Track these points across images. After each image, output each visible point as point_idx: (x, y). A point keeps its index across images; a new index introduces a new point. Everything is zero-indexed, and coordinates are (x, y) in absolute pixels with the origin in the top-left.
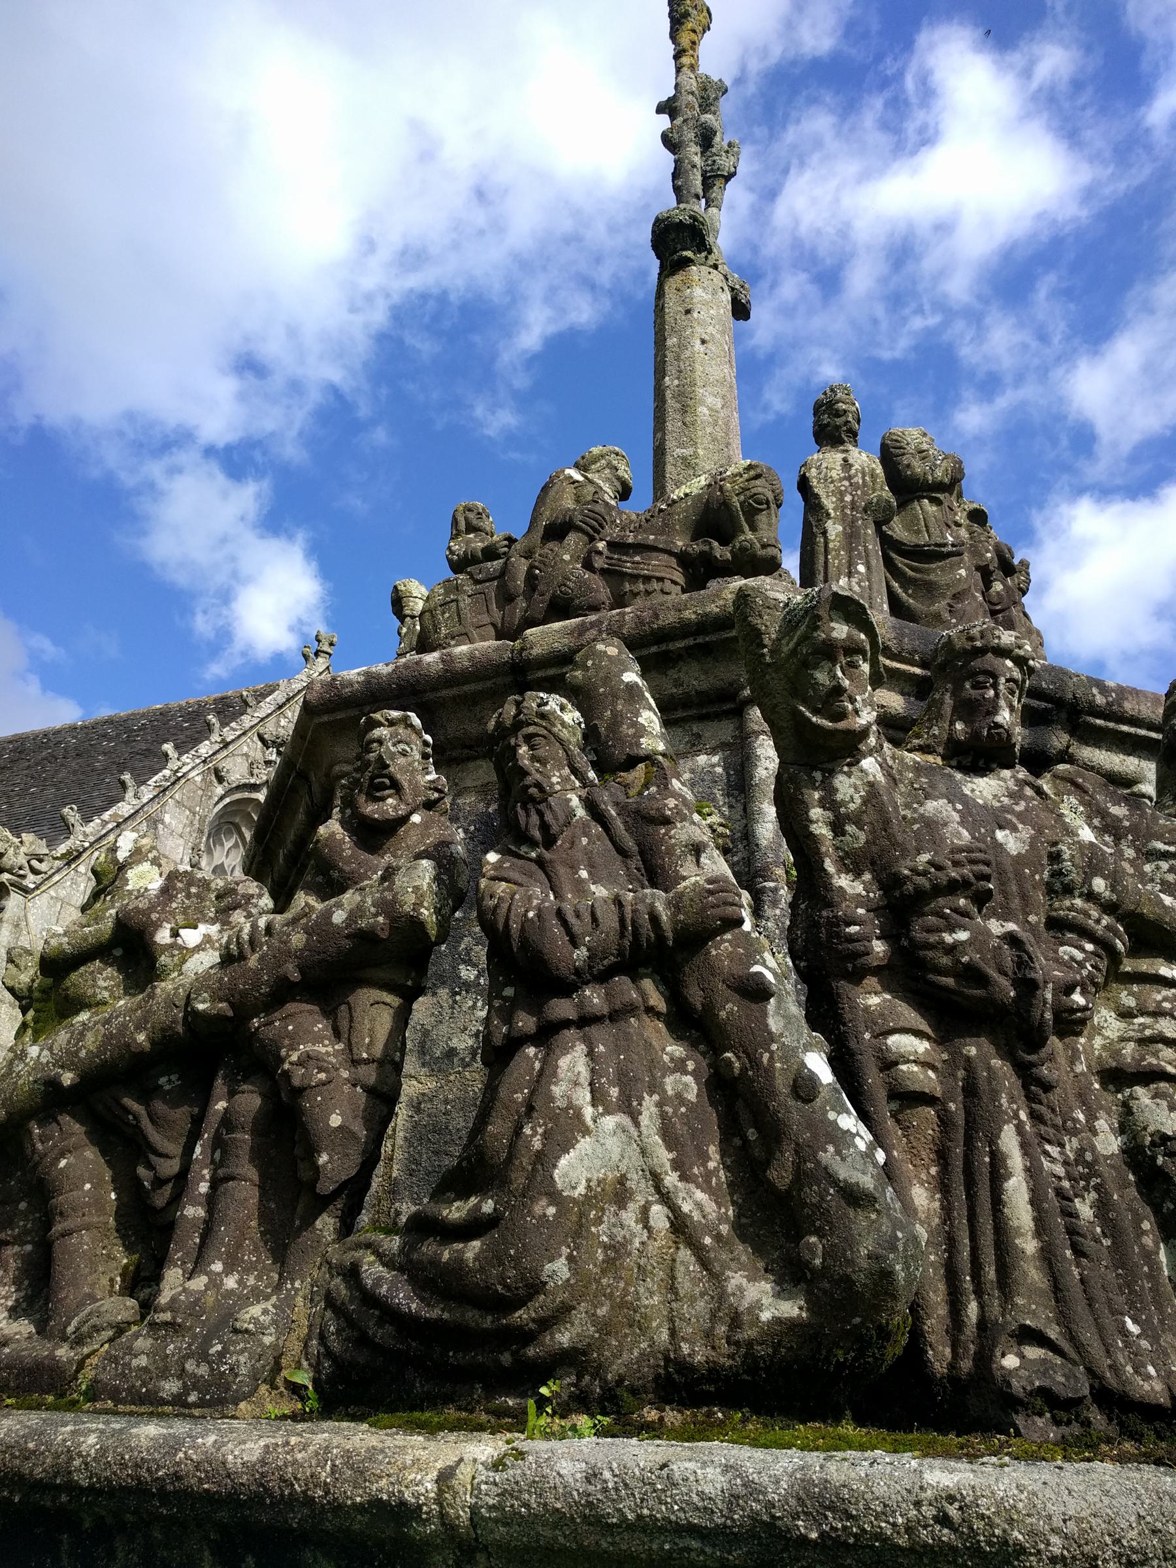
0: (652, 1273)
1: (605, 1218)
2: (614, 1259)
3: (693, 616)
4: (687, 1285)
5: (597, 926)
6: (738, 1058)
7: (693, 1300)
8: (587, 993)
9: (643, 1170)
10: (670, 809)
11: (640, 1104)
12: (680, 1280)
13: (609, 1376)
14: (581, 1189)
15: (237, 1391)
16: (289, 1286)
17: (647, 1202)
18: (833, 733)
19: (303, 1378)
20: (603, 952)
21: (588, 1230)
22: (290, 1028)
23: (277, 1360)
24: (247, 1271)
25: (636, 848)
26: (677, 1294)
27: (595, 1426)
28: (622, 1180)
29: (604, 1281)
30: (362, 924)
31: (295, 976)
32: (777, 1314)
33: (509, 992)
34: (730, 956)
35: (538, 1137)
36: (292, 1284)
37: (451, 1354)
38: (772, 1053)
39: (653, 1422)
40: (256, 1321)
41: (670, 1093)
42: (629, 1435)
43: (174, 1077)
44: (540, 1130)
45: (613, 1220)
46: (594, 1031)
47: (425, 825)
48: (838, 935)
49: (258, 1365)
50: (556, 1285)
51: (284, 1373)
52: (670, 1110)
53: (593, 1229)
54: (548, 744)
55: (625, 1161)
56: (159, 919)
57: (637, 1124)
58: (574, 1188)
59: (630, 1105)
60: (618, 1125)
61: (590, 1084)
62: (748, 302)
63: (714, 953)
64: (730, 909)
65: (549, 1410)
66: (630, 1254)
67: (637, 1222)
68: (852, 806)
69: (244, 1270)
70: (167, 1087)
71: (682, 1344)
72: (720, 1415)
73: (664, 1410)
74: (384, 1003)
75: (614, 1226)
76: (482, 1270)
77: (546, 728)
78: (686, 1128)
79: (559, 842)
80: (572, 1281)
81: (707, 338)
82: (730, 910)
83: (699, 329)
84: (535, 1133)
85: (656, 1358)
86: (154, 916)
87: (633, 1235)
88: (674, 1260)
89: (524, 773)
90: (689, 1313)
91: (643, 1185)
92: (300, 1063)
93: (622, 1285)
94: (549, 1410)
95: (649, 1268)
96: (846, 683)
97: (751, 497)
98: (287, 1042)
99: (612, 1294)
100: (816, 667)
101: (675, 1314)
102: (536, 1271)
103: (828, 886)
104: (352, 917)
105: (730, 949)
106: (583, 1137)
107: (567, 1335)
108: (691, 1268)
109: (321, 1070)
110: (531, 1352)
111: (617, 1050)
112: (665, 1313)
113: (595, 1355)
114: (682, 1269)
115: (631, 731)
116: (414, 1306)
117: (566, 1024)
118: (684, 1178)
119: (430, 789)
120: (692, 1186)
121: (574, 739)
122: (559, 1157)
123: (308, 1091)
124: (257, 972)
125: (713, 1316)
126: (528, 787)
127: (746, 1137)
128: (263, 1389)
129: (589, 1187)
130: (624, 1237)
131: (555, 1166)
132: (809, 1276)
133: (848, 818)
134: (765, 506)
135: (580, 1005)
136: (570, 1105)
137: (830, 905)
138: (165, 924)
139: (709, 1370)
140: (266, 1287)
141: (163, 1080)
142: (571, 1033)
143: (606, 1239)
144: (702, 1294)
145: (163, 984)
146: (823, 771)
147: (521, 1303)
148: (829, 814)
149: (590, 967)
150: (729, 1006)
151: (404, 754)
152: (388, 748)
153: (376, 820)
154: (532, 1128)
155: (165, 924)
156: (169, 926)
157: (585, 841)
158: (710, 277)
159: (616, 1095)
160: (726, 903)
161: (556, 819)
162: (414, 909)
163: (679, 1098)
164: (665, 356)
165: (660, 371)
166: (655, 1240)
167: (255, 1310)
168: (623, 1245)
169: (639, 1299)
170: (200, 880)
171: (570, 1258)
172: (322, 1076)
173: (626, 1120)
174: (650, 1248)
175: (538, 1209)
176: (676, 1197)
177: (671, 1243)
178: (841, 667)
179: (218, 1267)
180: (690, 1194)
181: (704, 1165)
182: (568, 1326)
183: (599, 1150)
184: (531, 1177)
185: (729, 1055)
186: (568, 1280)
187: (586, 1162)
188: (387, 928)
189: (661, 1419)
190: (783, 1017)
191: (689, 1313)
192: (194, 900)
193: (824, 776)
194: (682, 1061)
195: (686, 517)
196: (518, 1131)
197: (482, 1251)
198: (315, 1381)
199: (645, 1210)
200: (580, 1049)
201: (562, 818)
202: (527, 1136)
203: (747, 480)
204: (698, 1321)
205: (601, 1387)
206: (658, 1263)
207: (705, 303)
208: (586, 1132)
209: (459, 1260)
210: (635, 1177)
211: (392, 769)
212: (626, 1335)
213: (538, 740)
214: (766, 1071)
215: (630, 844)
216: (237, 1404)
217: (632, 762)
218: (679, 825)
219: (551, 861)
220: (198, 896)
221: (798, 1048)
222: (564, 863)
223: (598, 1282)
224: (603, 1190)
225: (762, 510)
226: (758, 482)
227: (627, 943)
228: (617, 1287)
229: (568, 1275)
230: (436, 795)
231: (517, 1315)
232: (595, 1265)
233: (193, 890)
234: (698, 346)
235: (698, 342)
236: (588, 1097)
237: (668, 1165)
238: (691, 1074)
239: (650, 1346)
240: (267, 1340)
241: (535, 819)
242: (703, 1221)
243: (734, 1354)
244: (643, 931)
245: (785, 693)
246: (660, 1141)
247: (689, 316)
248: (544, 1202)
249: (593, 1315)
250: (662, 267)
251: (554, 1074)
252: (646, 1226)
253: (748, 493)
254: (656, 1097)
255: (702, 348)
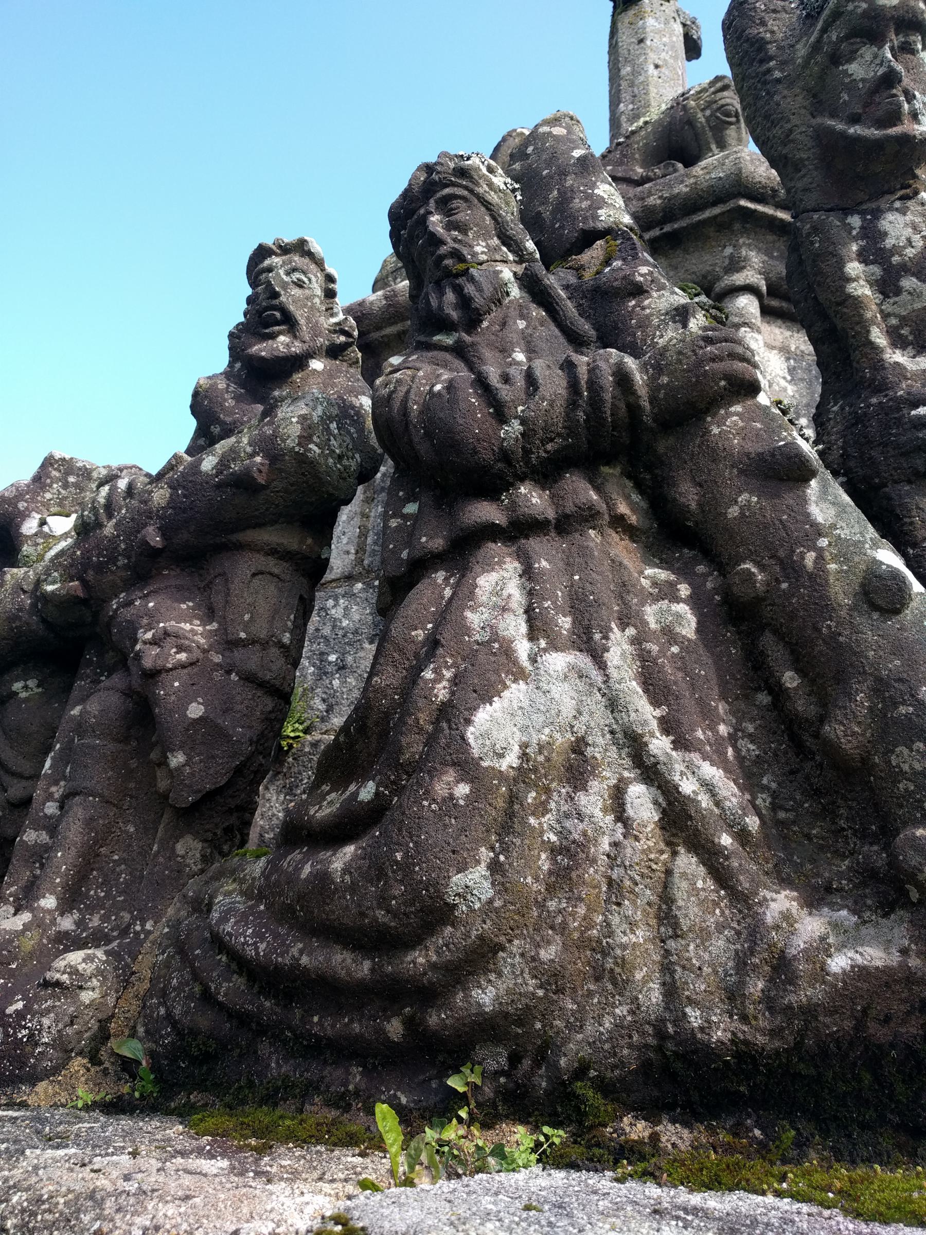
0: (632, 892)
1: (553, 805)
2: (568, 868)
3: (659, 202)
4: (694, 911)
5: (536, 389)
6: (762, 567)
7: (704, 936)
8: (523, 490)
9: (612, 732)
10: (642, 275)
11: (606, 637)
12: (680, 903)
13: (563, 1062)
14: (512, 759)
15: (34, 1067)
16: (138, 928)
17: (621, 780)
18: (878, 145)
19: (132, 1049)
20: (545, 429)
21: (524, 823)
22: (151, 604)
23: (104, 1024)
24: (91, 909)
25: (593, 333)
26: (676, 925)
27: (538, 1144)
28: (579, 746)
29: (552, 905)
30: (235, 467)
31: (156, 540)
32: (859, 960)
33: (411, 508)
34: (741, 432)
35: (445, 683)
36: (143, 925)
37: (316, 1019)
38: (820, 552)
39: (641, 1142)
40: (73, 971)
41: (653, 626)
42: (595, 1165)
43: (31, 683)
44: (448, 674)
45: (565, 808)
46: (534, 544)
47: (329, 374)
48: (899, 422)
49: (69, 1031)
50: (472, 910)
51: (112, 1043)
52: (654, 648)
53: (532, 821)
54: (469, 208)
55: (584, 718)
56: (27, 508)
57: (601, 665)
58: (501, 756)
59: (590, 639)
60: (572, 667)
61: (526, 612)
62: (699, 38)
63: (715, 430)
64: (740, 366)
65: (463, 1114)
66: (594, 861)
67: (605, 810)
68: (910, 252)
69: (87, 907)
70: (23, 695)
71: (688, 1010)
72: (757, 1132)
73: (659, 1122)
74: (271, 574)
75: (567, 816)
76: (353, 888)
77: (466, 188)
78: (680, 675)
79: (485, 324)
80: (498, 903)
81: (660, 63)
82: (740, 366)
83: (653, 57)
84: (439, 678)
85: (643, 1034)
86: (22, 505)
87: (599, 831)
88: (669, 872)
89: (436, 241)
90: (699, 958)
91: (613, 752)
92: (154, 642)
93: (582, 910)
94: (463, 1114)
95: (628, 883)
96: (899, 68)
97: (719, 109)
98: (145, 621)
99: (564, 926)
100: (851, 57)
101: (674, 958)
102: (437, 887)
103: (879, 365)
104: (223, 464)
105: (741, 424)
106: (515, 681)
107: (491, 992)
108: (700, 884)
109: (180, 649)
110: (434, 1019)
111: (569, 567)
112: (657, 958)
113: (538, 1026)
114: (684, 885)
115: (585, 204)
116: (262, 946)
117: (490, 532)
118: (680, 744)
119: (335, 332)
120: (695, 757)
121: (510, 210)
122: (476, 709)
123: (164, 675)
124: (113, 540)
125: (742, 964)
126: (442, 258)
127: (780, 685)
128: (78, 1064)
129: (524, 756)
130: (585, 834)
131: (468, 722)
132: (914, 895)
133: (906, 269)
134: (733, 119)
135: (513, 506)
136: (495, 637)
137: (881, 387)
138: (34, 514)
139: (739, 1056)
140: (112, 930)
141: (17, 686)
142: (495, 548)
143: (553, 838)
144: (720, 928)
145: (15, 570)
146: (862, 213)
147: (415, 940)
148: (876, 270)
149: (527, 452)
150: (743, 498)
151: (299, 285)
152: (278, 274)
153: (263, 358)
154: (435, 671)
155: (34, 514)
156: (38, 516)
157: (521, 324)
158: (663, 8)
159: (567, 626)
160: (733, 356)
161: (480, 290)
162: (299, 444)
163: (669, 634)
164: (620, 85)
165: (615, 100)
166: (637, 839)
167: (75, 957)
168: (582, 846)
169: (611, 934)
170: (80, 469)
171: (495, 867)
172: (183, 656)
173: (584, 661)
174: (629, 851)
175: (440, 789)
176: (670, 771)
177: (662, 846)
178: (892, 49)
179: (49, 902)
180: (692, 769)
181: (713, 728)
182: (493, 977)
183: (541, 699)
184: (431, 740)
185: (747, 566)
186: (490, 901)
187: (519, 720)
188: (265, 469)
189: (655, 1138)
190: (833, 504)
191: (699, 958)
192: (73, 490)
193: (864, 220)
194: (672, 585)
195: (646, 145)
196: (415, 673)
197: (355, 857)
198: (152, 1054)
199: (618, 794)
200: (512, 567)
201: (488, 289)
202: (426, 682)
203: (715, 93)
204: (716, 972)
205: (549, 1079)
206: (642, 876)
207: (658, 32)
208: (520, 675)
209: (323, 878)
210: (600, 741)
211: (283, 299)
212: (590, 994)
213: (455, 203)
214: (811, 576)
215: (586, 327)
216: (34, 1085)
217: (589, 237)
218: (655, 294)
219: (473, 344)
220: (76, 485)
221: (864, 542)
222: (491, 345)
223: (541, 906)
224: (548, 760)
225: (731, 123)
226: (725, 93)
227: (581, 415)
228: (573, 915)
229: (490, 893)
230: (342, 339)
231: (409, 958)
232: (536, 879)
233: (72, 479)
234: (651, 69)
235: (652, 67)
236: (523, 628)
237: (654, 725)
238: (684, 601)
239: (632, 1012)
240: (86, 997)
241: (450, 296)
242: (716, 811)
243: (782, 1029)
244: (608, 396)
245: (803, 111)
246: (640, 690)
247: (642, 45)
248: (450, 776)
249: (533, 959)
250: (615, 8)
251: (471, 595)
252: (621, 816)
253: (715, 106)
254: (631, 631)
255: (656, 72)
